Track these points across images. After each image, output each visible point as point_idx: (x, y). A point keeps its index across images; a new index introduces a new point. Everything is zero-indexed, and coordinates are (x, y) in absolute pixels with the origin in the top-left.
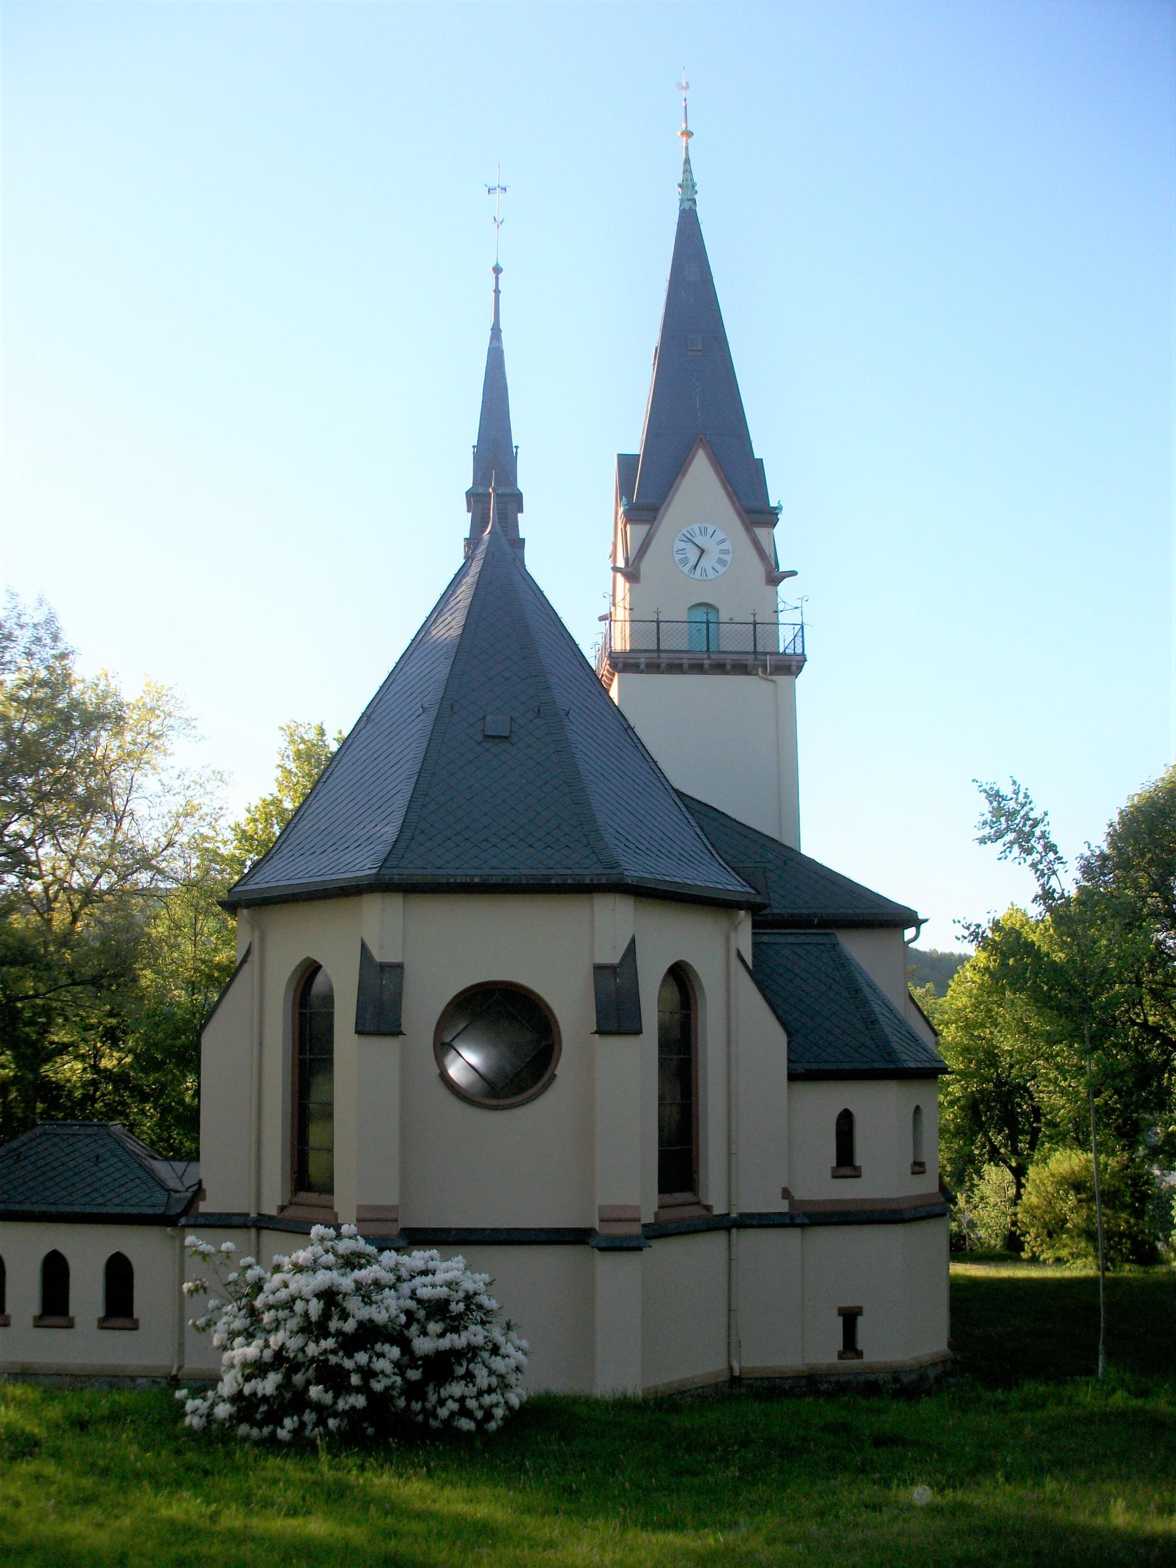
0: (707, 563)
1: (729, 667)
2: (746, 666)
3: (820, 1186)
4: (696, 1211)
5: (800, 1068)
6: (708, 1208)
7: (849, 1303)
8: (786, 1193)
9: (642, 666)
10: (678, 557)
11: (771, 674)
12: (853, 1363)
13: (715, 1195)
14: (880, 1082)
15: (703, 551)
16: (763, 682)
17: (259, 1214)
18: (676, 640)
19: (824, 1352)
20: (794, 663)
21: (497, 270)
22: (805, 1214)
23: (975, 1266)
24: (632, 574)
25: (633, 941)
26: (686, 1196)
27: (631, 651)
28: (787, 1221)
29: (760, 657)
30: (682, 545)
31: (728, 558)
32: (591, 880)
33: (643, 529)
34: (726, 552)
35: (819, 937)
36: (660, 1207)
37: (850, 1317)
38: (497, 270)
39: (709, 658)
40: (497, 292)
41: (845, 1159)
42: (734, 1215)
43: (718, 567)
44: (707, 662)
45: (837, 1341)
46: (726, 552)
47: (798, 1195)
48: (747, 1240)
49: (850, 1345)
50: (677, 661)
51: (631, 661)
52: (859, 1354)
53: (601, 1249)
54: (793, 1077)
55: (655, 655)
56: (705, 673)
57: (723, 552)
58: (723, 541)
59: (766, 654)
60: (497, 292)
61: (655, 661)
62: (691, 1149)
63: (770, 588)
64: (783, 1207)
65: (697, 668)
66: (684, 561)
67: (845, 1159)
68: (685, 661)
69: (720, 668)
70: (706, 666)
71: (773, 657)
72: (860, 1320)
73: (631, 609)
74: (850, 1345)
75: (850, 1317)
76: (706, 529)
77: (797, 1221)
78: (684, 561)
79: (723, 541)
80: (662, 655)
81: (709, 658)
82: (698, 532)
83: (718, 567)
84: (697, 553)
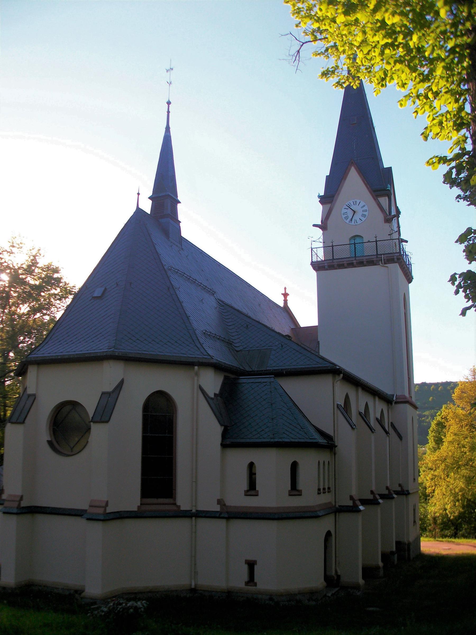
0: (357, 217)
1: (365, 262)
2: (373, 261)
3: (238, 499)
4: (174, 508)
5: (228, 442)
6: (179, 507)
7: (250, 558)
8: (220, 502)
9: (326, 267)
10: (343, 216)
11: (385, 263)
12: (251, 588)
13: (183, 500)
14: (262, 448)
15: (354, 212)
16: (383, 268)
17: (197, 511)
18: (344, 253)
19: (237, 580)
20: (395, 257)
21: (169, 103)
22: (228, 512)
23: (444, 552)
24: (323, 226)
25: (122, 382)
26: (170, 501)
27: (324, 260)
28: (218, 515)
29: (379, 256)
30: (346, 211)
31: (366, 213)
32: (119, 354)
33: (328, 206)
34: (366, 211)
35: (253, 379)
36: (141, 504)
37: (251, 565)
38: (169, 103)
39: (355, 260)
40: (168, 112)
41: (294, 489)
42: (194, 511)
43: (362, 218)
44: (354, 261)
45: (246, 577)
46: (366, 211)
47: (228, 503)
48: (203, 523)
49: (251, 580)
50: (341, 263)
51: (321, 265)
52: (255, 585)
53: (88, 519)
54: (224, 446)
55: (331, 261)
56: (346, 268)
57: (363, 211)
58: (364, 206)
59: (381, 255)
60: (168, 112)
61: (331, 264)
62: (172, 479)
63: (387, 225)
64: (217, 508)
65: (351, 265)
66: (346, 218)
67: (294, 489)
68: (345, 262)
69: (361, 264)
70: (355, 264)
71: (386, 256)
72: (256, 567)
73: (324, 242)
74: (251, 580)
75: (251, 565)
76: (356, 202)
77: (222, 515)
78: (346, 218)
79: (364, 206)
80: (334, 261)
81: (355, 260)
82: (352, 203)
83: (362, 218)
84: (352, 213)
